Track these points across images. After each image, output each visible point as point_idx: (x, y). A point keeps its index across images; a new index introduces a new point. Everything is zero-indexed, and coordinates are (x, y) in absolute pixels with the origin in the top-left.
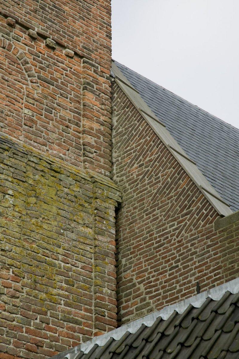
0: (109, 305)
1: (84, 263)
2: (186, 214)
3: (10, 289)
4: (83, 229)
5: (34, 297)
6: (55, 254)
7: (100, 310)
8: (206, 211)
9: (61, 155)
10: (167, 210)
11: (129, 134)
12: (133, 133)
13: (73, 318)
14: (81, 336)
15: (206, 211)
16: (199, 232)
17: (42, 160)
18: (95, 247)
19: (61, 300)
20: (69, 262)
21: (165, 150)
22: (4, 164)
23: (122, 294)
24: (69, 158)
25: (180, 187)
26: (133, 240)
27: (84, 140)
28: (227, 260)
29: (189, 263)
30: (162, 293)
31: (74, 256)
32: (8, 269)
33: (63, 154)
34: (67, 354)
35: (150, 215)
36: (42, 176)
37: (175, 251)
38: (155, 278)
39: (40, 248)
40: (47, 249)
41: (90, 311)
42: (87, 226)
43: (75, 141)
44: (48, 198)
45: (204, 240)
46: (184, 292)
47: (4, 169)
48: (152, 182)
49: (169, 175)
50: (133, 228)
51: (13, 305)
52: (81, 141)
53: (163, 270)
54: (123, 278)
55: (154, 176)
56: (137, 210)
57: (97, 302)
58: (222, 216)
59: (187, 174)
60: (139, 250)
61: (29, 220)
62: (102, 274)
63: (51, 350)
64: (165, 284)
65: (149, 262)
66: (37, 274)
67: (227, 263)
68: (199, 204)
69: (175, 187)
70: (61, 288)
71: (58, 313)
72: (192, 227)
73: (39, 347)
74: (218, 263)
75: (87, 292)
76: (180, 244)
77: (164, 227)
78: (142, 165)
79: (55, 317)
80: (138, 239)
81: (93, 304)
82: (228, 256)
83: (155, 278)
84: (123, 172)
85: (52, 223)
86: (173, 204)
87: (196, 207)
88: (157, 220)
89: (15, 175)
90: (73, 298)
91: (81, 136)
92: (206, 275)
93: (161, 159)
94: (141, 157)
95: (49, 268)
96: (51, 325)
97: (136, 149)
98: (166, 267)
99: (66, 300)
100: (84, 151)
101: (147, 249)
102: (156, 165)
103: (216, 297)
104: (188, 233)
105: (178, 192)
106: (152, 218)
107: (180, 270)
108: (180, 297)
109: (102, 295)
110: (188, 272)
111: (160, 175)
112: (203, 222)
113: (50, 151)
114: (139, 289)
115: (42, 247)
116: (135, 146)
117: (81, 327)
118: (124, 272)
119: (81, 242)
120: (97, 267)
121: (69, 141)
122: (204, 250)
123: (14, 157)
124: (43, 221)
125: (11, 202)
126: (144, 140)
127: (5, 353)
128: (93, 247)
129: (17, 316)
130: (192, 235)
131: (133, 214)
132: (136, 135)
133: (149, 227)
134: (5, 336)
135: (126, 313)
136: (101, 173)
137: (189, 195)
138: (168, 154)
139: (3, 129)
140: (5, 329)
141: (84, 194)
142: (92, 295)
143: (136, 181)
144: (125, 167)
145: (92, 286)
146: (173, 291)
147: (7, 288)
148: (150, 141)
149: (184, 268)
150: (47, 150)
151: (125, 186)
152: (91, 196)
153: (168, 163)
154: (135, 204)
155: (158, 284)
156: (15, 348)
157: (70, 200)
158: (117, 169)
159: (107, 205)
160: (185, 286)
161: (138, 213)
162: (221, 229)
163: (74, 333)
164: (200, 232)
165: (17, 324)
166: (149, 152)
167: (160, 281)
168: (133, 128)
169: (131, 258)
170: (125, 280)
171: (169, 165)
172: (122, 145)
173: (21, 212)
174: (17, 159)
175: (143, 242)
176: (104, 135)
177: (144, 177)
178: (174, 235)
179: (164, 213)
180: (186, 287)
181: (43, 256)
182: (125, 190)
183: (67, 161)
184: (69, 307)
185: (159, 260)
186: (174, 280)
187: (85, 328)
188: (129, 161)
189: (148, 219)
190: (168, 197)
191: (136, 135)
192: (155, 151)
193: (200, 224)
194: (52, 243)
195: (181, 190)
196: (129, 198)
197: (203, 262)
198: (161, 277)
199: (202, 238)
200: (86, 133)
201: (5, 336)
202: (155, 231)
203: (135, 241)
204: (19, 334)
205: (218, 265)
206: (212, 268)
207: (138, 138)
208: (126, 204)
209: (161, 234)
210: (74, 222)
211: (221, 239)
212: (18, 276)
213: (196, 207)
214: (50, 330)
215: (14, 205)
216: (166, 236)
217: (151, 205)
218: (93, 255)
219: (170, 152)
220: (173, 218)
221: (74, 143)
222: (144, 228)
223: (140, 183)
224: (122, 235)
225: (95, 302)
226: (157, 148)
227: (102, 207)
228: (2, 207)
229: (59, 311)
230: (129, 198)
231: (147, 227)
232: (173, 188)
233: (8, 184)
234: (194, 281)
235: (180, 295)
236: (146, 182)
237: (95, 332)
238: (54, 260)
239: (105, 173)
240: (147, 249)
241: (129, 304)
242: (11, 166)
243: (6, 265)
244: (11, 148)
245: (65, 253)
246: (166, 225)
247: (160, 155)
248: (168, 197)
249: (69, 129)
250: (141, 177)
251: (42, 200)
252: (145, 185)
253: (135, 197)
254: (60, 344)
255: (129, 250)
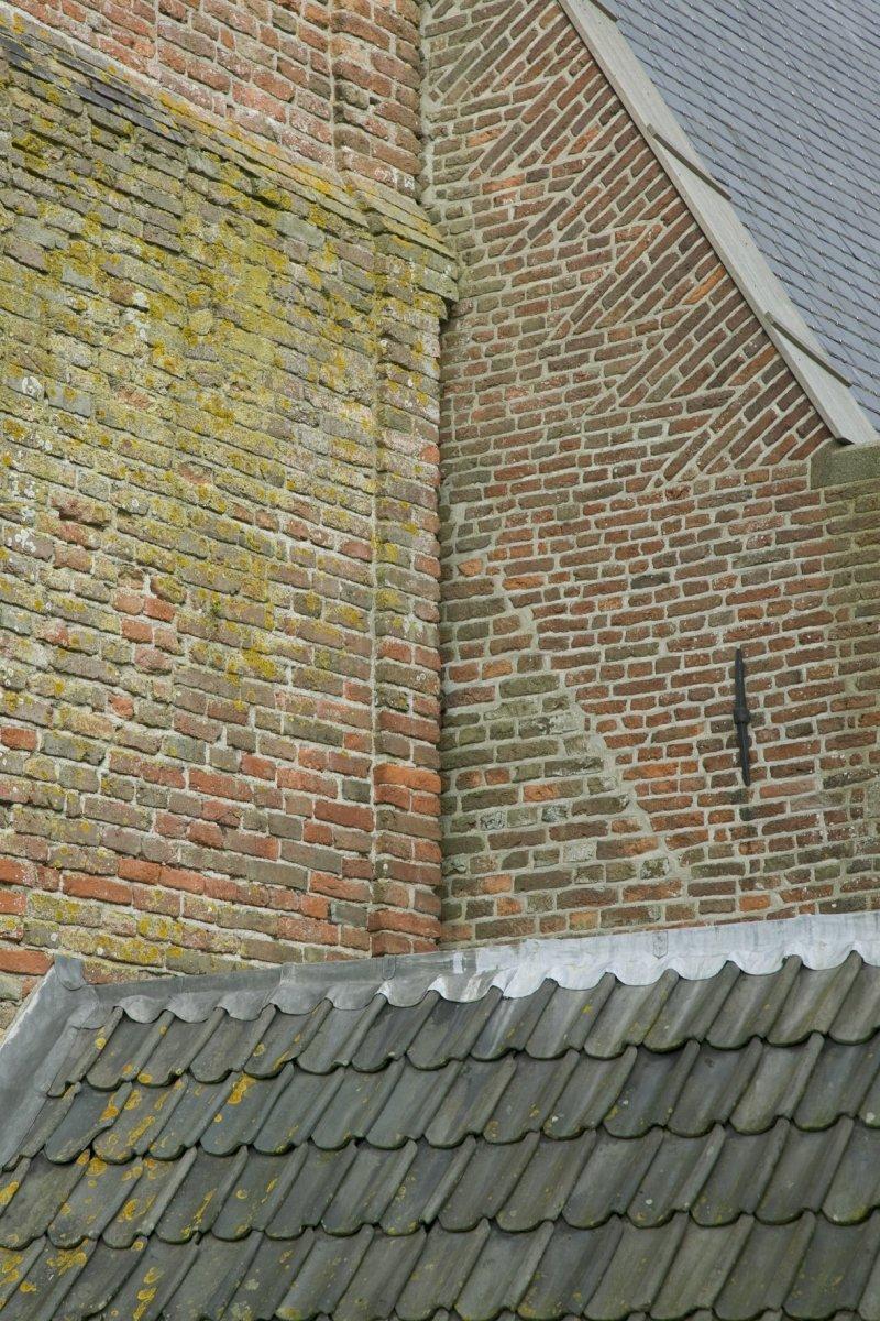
1: (349, 531)
2: (708, 403)
3: (146, 646)
5: (213, 665)
7: (394, 691)
8: (784, 410)
9: (271, 121)
10: (635, 368)
11: (491, 38)
12: (505, 39)
13: (318, 725)
14: (339, 779)
15: (784, 410)
17: (227, 164)
18: (379, 472)
19: (286, 666)
21: (633, 142)
23: (449, 624)
24: (293, 133)
25: (685, 297)
26: (498, 445)
27: (341, 58)
28: (852, 599)
29: (709, 578)
30: (603, 655)
31: (322, 511)
32: (138, 577)
33: (276, 119)
34: (433, 979)
35: (565, 372)
36: (229, 224)
37: (658, 525)
38: (576, 599)
40: (246, 496)
41: (359, 694)
42: (357, 400)
43: (313, 62)
44: (247, 307)
45: (770, 510)
46: (683, 670)
47: (118, 211)
49: (648, 244)
50: (499, 404)
51: (156, 700)
52: (330, 60)
53: (608, 579)
54: (456, 572)
55: (586, 231)
56: (515, 341)
57: (388, 664)
58: (844, 442)
59: (716, 255)
60: (517, 489)
61: (193, 394)
63: (259, 834)
65: (556, 538)
66: (219, 587)
67: (852, 608)
68: (757, 378)
69: (669, 294)
70: (286, 627)
72: (725, 453)
73: (228, 830)
75: (357, 633)
76: (678, 502)
77: (618, 429)
78: (541, 175)
79: (271, 726)
80: (519, 448)
81: (373, 671)
82: (854, 585)
83: (576, 599)
84: (462, 184)
85: (260, 398)
86: (657, 355)
88: (594, 398)
89: (153, 229)
90: (317, 657)
91: (329, 39)
93: (616, 171)
94: (536, 145)
96: (258, 755)
100: (338, 99)
101: (550, 492)
102: (597, 191)
104: (709, 473)
106: (572, 386)
107: (673, 592)
108: (668, 682)
109: (399, 641)
110: (702, 605)
111: (609, 230)
113: (240, 110)
114: (515, 623)
115: (232, 490)
116: (515, 94)
117: (339, 750)
118: (460, 551)
119: (340, 459)
120: (386, 546)
121: (295, 63)
122: (768, 544)
123: (146, 160)
124: (234, 394)
125: (143, 334)
126: (552, 80)
128: (372, 472)
129: (167, 733)
130: (723, 483)
131: (498, 349)
132: (517, 51)
134: (134, 803)
135: (465, 692)
136: (388, 183)
138: (644, 162)
139: (99, 36)
143: (514, 230)
144: (473, 166)
146: (644, 659)
147: (138, 642)
149: (690, 589)
150: (228, 106)
151: (470, 238)
153: (642, 195)
154: (507, 317)
156: (163, 840)
157: (310, 308)
158: (437, 165)
160: (690, 653)
161: (517, 352)
163: (319, 773)
164: (757, 478)
165: (168, 760)
166: (567, 133)
167: (597, 613)
168: (508, 20)
169: (489, 510)
170: (461, 579)
171: (649, 205)
172: (461, 78)
174: (156, 169)
175: (536, 462)
176: (399, 31)
177: (545, 222)
178: (657, 465)
179: (620, 379)
184: (307, 688)
186: (650, 623)
187: (349, 751)
188: (488, 146)
190: (639, 322)
191: (517, 51)
192: (592, 133)
193: (758, 451)
194: (259, 474)
197: (762, 586)
200: (348, 29)
201: (134, 803)
202: (583, 432)
203: (504, 452)
204: (175, 794)
205: (816, 610)
206: (793, 614)
207: (528, 67)
208: (471, 309)
209: (606, 449)
210: (321, 388)
214: (257, 769)
215: (150, 346)
216: (626, 463)
217: (570, 337)
218: (373, 500)
219: (652, 155)
220: (654, 405)
222: (540, 414)
223: (530, 243)
225: (378, 662)
226: (604, 124)
227: (404, 327)
229: (280, 706)
232: (658, 295)
233: (131, 267)
234: (725, 641)
235: (668, 676)
236: (555, 245)
237: (380, 763)
238: (265, 532)
239: (401, 181)
240: (550, 492)
242: (138, 198)
243: (134, 563)
244: (136, 125)
245: (297, 501)
247: (611, 156)
248: (639, 322)
249: (293, 14)
250: (533, 220)
251: (229, 317)
252: (548, 256)
253: (508, 289)
254: (282, 813)
255: (483, 477)
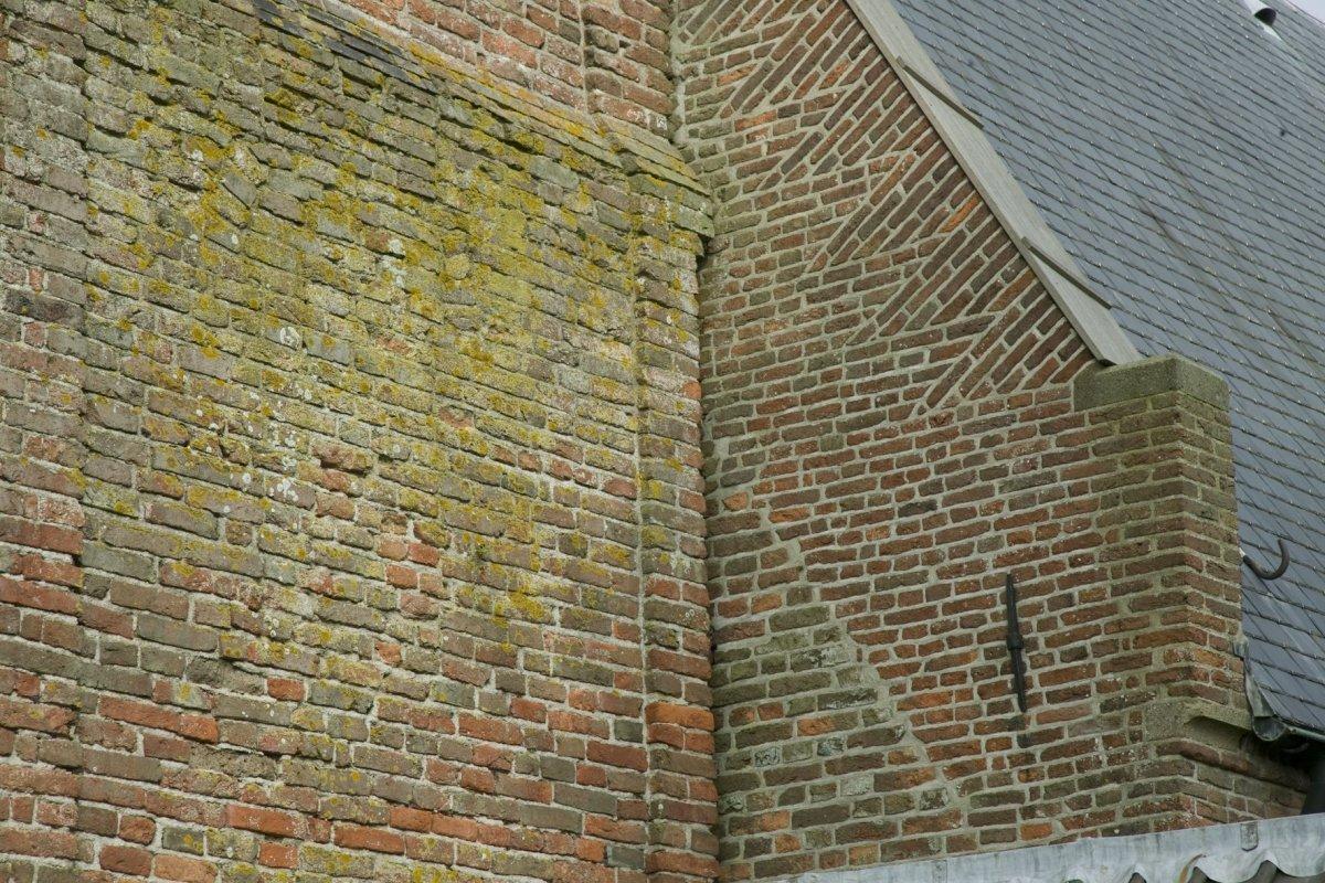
0: (688, 609)
1: (613, 469)
2: (968, 329)
3: (411, 592)
4: (604, 348)
5: (479, 609)
6: (530, 451)
7: (663, 629)
8: (1044, 333)
9: (522, 67)
10: (893, 298)
14: (610, 719)
15: (1044, 333)
16: (1016, 403)
18: (641, 410)
20: (567, 474)
22: (372, 141)
23: (716, 559)
24: (545, 78)
25: (942, 226)
26: (759, 378)
28: (1121, 519)
29: (976, 504)
31: (585, 450)
32: (401, 522)
33: (527, 65)
36: (483, 169)
39: (489, 437)
40: (507, 438)
43: (562, 8)
44: (504, 250)
46: (953, 597)
47: (372, 160)
48: (831, 182)
49: (902, 174)
51: (423, 645)
53: (875, 508)
54: (721, 507)
55: (840, 164)
56: (773, 275)
58: (1106, 364)
60: (780, 421)
61: (451, 339)
62: (665, 505)
63: (532, 778)
64: (885, 558)
65: (821, 469)
66: (483, 530)
67: (1122, 529)
69: (925, 222)
71: (544, 653)
72: (987, 379)
74: (1086, 524)
76: (942, 429)
77: (879, 358)
78: (793, 110)
79: (540, 668)
80: (780, 381)
81: (641, 609)
82: (1122, 506)
86: (915, 284)
87: (1005, 311)
88: (854, 328)
89: (407, 177)
92: (1040, 557)
93: (867, 103)
94: (787, 81)
95: (514, 502)
96: (527, 697)
97: (767, 43)
98: (887, 500)
99: (567, 605)
100: (588, 43)
101: (813, 423)
102: (848, 124)
103: (1291, 864)
104: (972, 398)
105: (936, 242)
106: (831, 317)
107: (940, 520)
108: (939, 610)
109: (666, 578)
110: (969, 531)
111: (863, 162)
112: (1030, 368)
113: (490, 57)
114: (783, 556)
116: (765, 32)
118: (726, 486)
121: (544, 10)
122: (1034, 468)
123: (398, 109)
124: (492, 337)
125: (400, 281)
126: (800, 17)
127: (407, 806)
128: (634, 410)
129: (435, 678)
130: (986, 408)
131: (756, 283)
133: (821, 347)
134: (404, 750)
135: (735, 627)
136: (641, 124)
137: (977, 264)
140: (402, 727)
141: (604, 219)
142: (637, 579)
145: (634, 547)
147: (403, 588)
148: (824, 27)
149: (958, 515)
150: (479, 54)
152: (626, 223)
153: (894, 127)
154: (764, 252)
155: (858, 552)
156: (434, 787)
157: (566, 250)
158: (688, 106)
159: (673, 253)
160: (960, 580)
162: (1099, 409)
163: (590, 714)
165: (436, 705)
166: (817, 68)
167: (865, 542)
169: (752, 443)
170: (727, 514)
172: (711, 18)
173: (428, 314)
174: (408, 118)
177: (798, 157)
178: (919, 393)
179: (879, 309)
180: (962, 583)
181: (498, 464)
182: (723, 191)
183: (539, 91)
185: (860, 470)
186: (919, 551)
187: (620, 691)
188: (739, 84)
189: (815, 318)
190: (896, 251)
192: (842, 68)
193: (1020, 375)
194: (520, 415)
195: (949, 236)
196: (742, 226)
197: (1029, 510)
198: (868, 531)
199: (1025, 424)
201: (404, 750)
202: (844, 363)
206: (1062, 537)
208: (727, 245)
209: (868, 379)
210: (580, 328)
211: (1099, 441)
212: (432, 544)
213: (1005, 311)
217: (827, 269)
221: (557, 16)
223: (784, 177)
224: (714, 354)
225: (646, 600)
226: (854, 58)
227: (661, 264)
228: (376, 304)
230: (742, 226)
231: (813, 344)
232: (914, 225)
233: (387, 215)
234: (995, 567)
235: (939, 603)
236: (809, 178)
238: (526, 472)
239: (653, 121)
240: (813, 423)
241: (746, 599)
242: (391, 148)
243: (397, 509)
244: (388, 76)
245: (559, 442)
246: (888, 354)
247: (862, 89)
248: (896, 251)
250: (786, 155)
251: (485, 260)
252: (803, 190)
253: (764, 224)
254: (554, 756)
255: (746, 411)
